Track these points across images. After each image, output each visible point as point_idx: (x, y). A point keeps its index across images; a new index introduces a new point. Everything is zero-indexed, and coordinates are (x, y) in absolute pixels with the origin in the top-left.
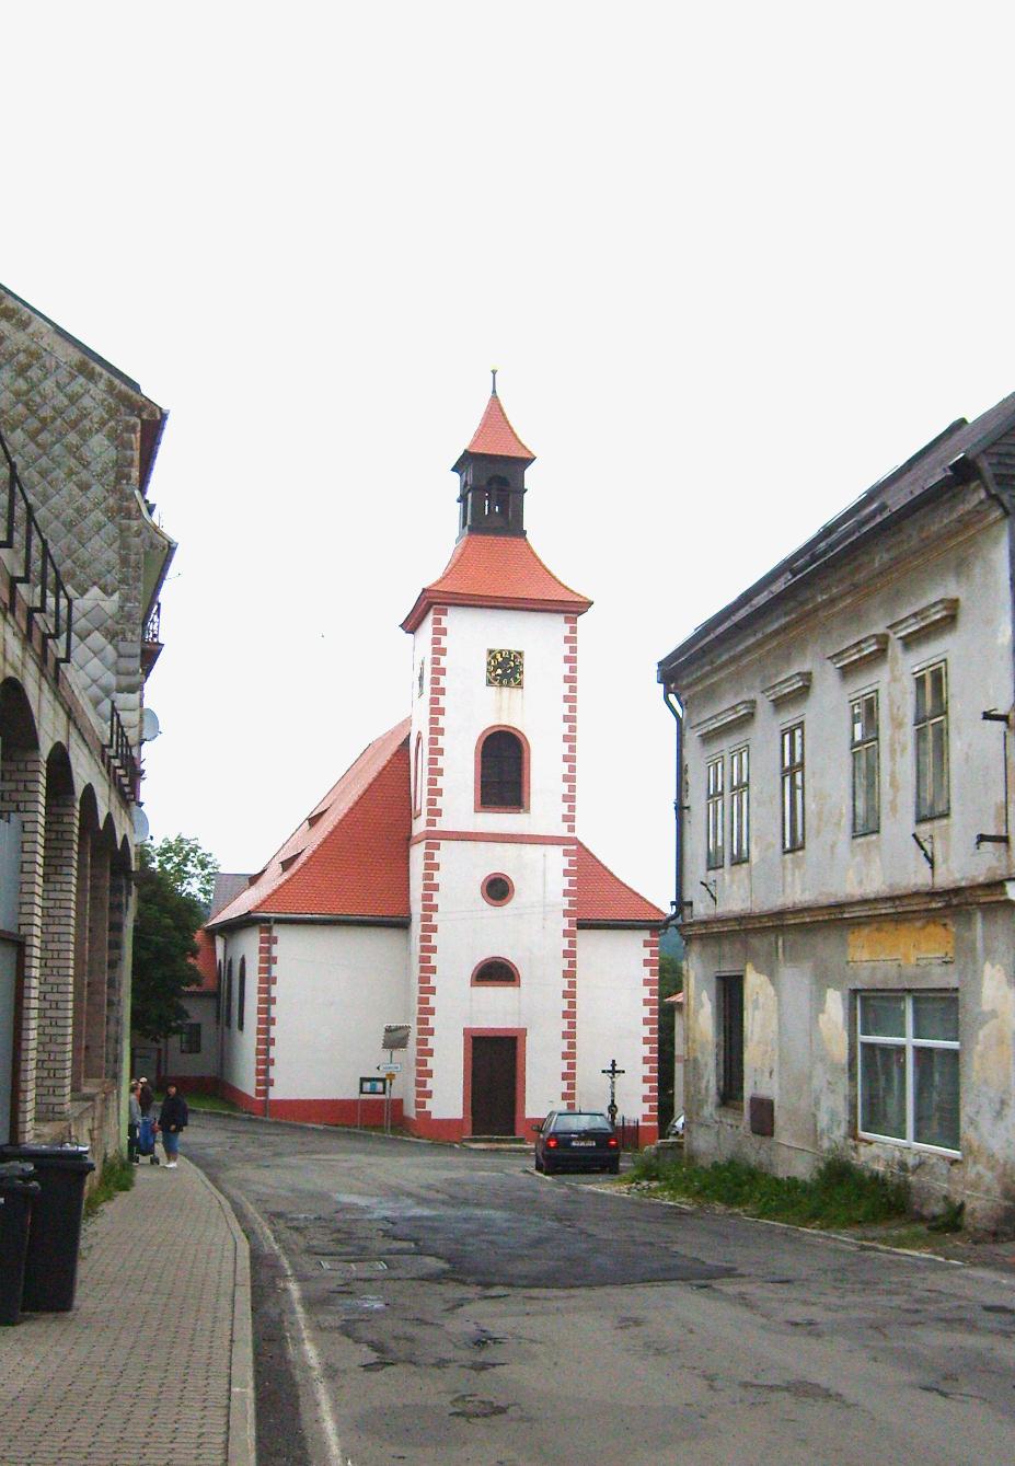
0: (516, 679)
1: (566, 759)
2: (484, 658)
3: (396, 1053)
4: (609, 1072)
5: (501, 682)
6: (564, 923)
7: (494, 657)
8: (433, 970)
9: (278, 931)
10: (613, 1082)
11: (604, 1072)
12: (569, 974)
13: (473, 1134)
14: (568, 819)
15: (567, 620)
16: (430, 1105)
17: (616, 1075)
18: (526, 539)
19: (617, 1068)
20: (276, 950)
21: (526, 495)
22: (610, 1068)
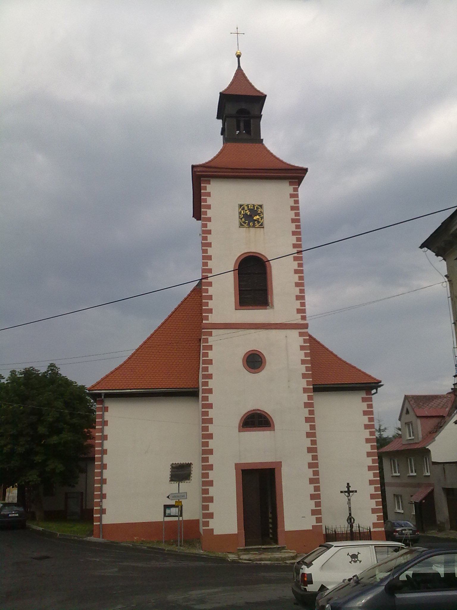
0: (259, 222)
3: (184, 486)
4: (345, 492)
5: (249, 224)
7: (243, 209)
10: (349, 500)
11: (341, 492)
14: (301, 311)
15: (291, 184)
17: (351, 494)
18: (263, 144)
19: (351, 489)
22: (346, 490)
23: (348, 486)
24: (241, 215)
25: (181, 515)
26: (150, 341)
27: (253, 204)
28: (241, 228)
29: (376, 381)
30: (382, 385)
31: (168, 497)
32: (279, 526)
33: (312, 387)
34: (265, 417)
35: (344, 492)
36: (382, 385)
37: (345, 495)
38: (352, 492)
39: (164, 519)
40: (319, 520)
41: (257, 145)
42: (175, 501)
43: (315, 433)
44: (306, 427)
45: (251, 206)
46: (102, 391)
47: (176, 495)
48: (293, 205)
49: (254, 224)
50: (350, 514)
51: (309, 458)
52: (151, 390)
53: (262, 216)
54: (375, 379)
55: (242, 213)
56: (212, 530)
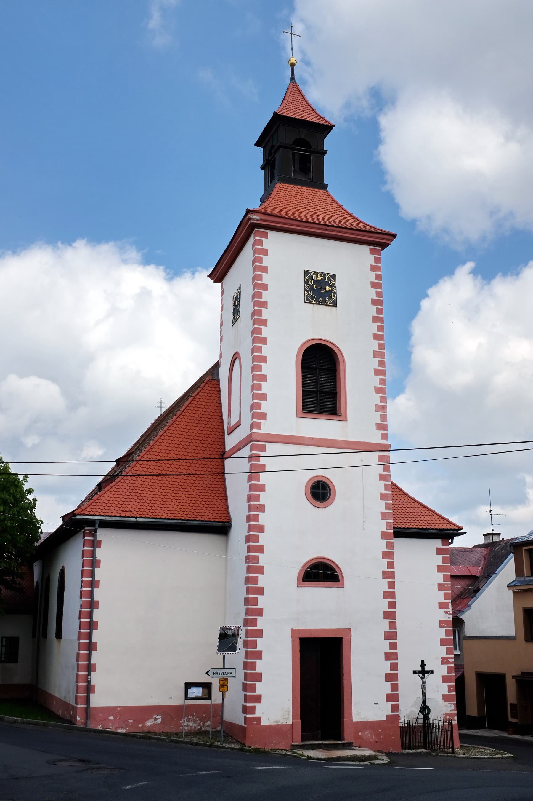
0: (330, 298)
1: (377, 372)
2: (301, 279)
3: (229, 656)
4: (419, 672)
6: (382, 526)
7: (311, 278)
8: (260, 570)
9: (102, 534)
10: (424, 683)
11: (414, 672)
12: (388, 575)
13: (302, 741)
14: (382, 427)
15: (372, 252)
16: (260, 710)
17: (426, 675)
18: (327, 191)
19: (426, 669)
20: (100, 554)
21: (326, 157)
22: (420, 669)
23: (423, 664)
24: (308, 287)
25: (210, 698)
26: (154, 450)
27: (323, 273)
28: (307, 304)
29: (457, 528)
30: (464, 533)
31: (207, 673)
32: (346, 714)
33: (392, 531)
34: (332, 569)
35: (417, 672)
36: (464, 533)
37: (419, 676)
38: (428, 672)
39: (184, 702)
40: (395, 708)
41: (320, 192)
42: (219, 678)
43: (394, 593)
44: (384, 585)
45: (321, 275)
46: (96, 518)
47: (219, 671)
48: (374, 280)
49: (324, 300)
50: (424, 702)
51: (385, 626)
52: (169, 521)
53: (335, 290)
54: (455, 525)
55: (309, 283)
56: (259, 719)
